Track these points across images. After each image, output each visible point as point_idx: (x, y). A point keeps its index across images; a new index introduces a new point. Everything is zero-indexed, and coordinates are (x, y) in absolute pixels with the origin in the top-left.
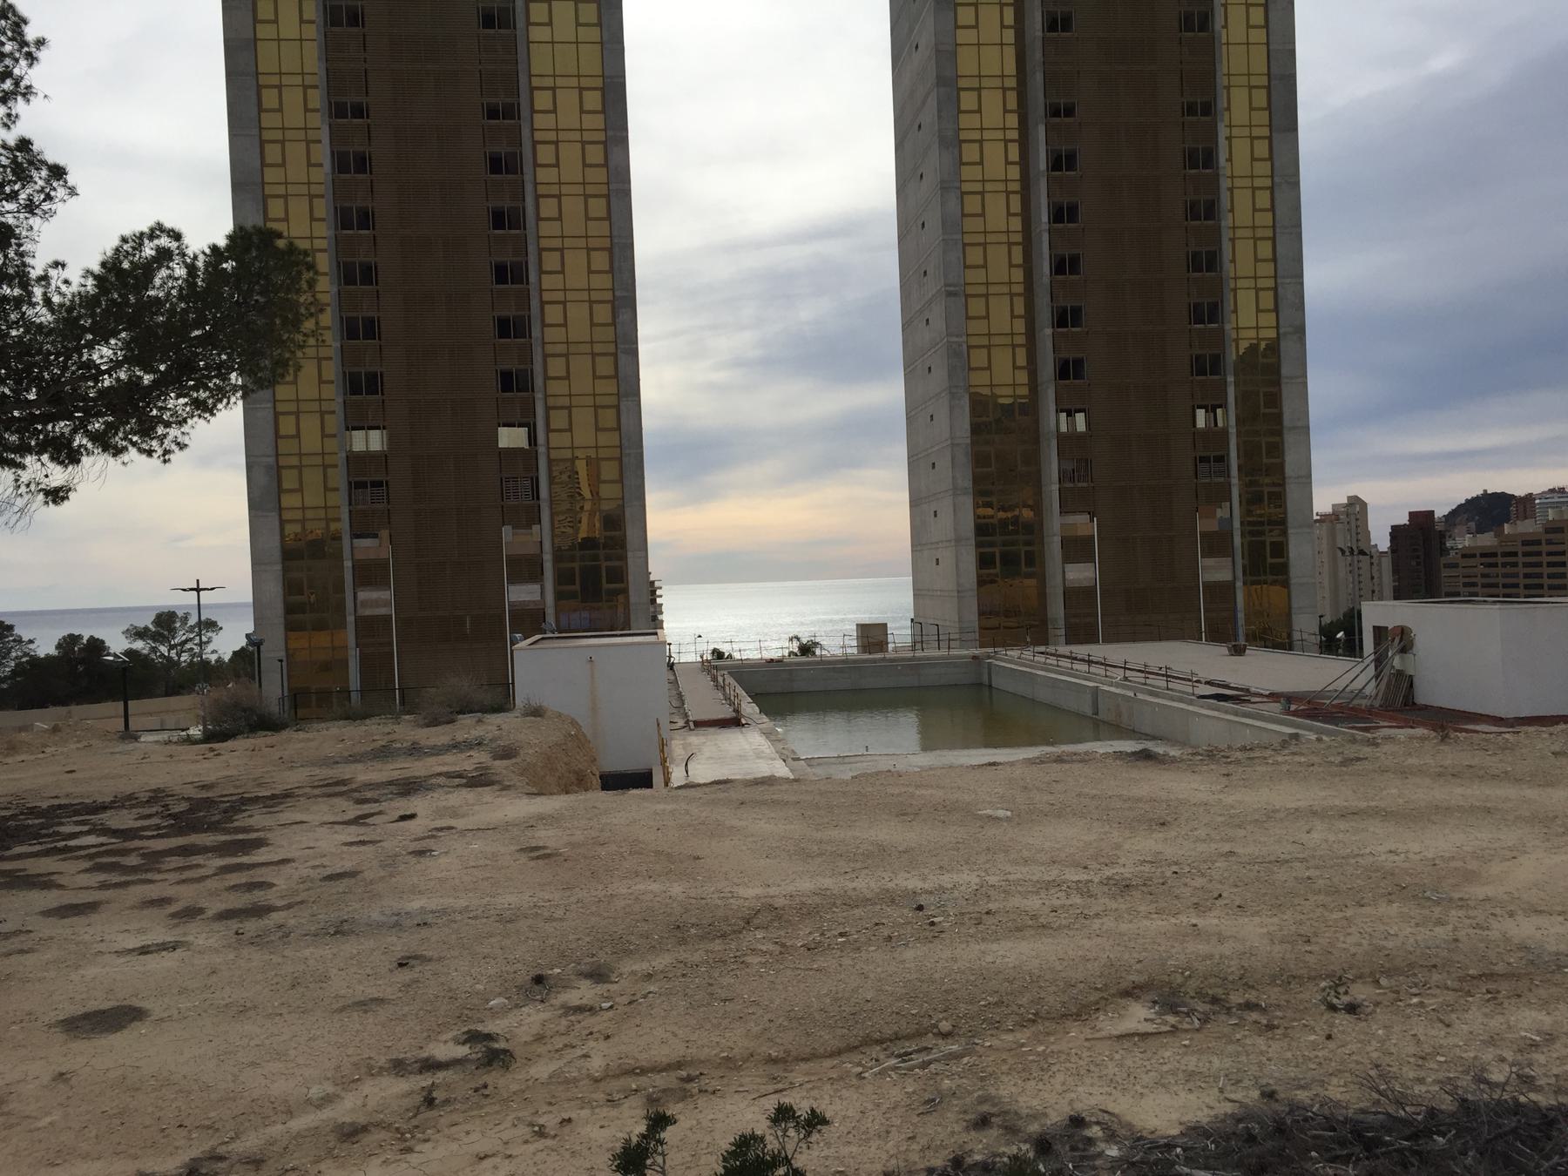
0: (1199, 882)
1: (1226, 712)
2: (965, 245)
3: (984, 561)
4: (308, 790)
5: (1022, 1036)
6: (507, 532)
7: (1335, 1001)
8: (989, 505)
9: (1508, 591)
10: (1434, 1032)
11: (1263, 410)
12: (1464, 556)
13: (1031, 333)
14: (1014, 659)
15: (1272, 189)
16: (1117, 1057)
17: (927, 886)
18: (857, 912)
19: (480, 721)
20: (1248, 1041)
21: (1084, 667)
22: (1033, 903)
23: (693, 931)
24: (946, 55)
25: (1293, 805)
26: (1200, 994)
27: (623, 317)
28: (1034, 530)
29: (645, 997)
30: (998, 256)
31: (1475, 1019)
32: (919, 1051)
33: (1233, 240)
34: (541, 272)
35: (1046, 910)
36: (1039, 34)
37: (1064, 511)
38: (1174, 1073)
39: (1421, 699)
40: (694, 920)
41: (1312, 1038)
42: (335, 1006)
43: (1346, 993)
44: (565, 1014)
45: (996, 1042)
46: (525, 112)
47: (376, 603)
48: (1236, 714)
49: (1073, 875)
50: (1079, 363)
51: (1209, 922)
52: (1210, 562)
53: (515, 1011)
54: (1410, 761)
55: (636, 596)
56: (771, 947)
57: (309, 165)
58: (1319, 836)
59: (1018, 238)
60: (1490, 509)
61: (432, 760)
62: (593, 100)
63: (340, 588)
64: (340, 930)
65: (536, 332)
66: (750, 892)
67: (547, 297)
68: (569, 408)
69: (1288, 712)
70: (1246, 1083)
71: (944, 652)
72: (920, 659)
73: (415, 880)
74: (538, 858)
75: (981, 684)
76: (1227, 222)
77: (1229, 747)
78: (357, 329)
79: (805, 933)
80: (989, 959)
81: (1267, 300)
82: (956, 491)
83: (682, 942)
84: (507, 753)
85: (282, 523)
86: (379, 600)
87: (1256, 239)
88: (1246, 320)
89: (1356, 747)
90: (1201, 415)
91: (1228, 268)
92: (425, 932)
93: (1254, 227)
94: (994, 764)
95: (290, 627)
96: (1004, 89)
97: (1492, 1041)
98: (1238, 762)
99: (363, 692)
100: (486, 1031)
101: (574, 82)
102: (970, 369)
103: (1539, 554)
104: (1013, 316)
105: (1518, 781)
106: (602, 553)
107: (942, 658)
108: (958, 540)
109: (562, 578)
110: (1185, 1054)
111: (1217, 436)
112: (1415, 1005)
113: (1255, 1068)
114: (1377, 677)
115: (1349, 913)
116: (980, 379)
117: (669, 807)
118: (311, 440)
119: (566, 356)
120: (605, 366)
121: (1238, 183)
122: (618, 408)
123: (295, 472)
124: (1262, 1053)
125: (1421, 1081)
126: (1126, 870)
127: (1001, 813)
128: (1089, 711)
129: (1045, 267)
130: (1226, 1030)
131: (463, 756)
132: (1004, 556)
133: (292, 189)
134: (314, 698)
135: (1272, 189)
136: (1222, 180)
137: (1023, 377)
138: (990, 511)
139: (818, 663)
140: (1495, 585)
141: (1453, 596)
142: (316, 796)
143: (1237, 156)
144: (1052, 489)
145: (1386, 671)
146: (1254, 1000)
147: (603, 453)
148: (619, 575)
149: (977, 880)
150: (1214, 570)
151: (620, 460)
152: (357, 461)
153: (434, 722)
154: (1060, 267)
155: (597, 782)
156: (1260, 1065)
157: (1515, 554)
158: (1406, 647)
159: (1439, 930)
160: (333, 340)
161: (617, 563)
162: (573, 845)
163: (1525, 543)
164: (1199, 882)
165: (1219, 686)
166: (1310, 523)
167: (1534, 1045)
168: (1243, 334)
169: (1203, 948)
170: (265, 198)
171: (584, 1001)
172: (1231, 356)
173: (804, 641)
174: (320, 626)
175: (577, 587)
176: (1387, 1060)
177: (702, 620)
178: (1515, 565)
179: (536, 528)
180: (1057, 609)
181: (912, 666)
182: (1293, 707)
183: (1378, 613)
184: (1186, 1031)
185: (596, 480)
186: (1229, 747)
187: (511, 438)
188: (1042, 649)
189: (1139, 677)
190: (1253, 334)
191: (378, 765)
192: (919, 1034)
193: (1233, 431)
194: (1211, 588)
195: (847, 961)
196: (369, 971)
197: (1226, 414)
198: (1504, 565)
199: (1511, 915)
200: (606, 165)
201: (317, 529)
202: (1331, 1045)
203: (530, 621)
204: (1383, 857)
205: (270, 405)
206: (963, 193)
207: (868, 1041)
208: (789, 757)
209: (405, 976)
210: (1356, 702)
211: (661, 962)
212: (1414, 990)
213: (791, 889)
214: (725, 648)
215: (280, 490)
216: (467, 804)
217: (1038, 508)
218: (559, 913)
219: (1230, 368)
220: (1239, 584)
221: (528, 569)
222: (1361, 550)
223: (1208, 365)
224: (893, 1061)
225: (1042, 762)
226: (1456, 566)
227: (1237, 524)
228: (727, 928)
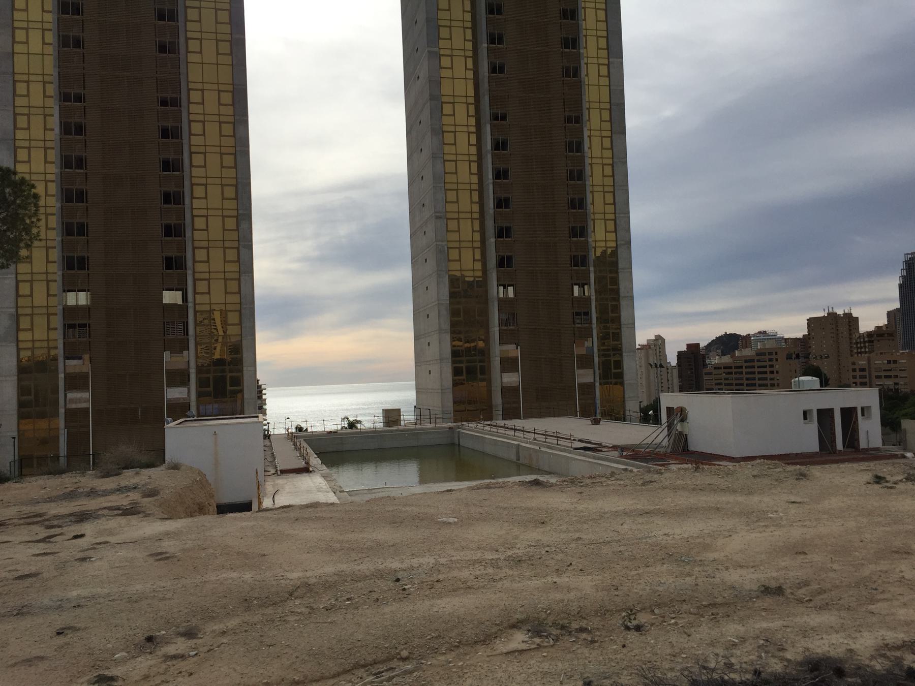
1: (589, 457)
2: (446, 190)
3: (456, 372)
4: (15, 521)
5: (450, 657)
6: (167, 355)
7: (629, 624)
9: (738, 387)
10: (682, 640)
12: (715, 368)
13: (483, 241)
14: (474, 429)
15: (612, 165)
16: (504, 666)
17: (404, 566)
18: (360, 584)
19: (137, 473)
20: (579, 651)
21: (512, 433)
22: (465, 574)
23: (255, 602)
24: (435, 82)
25: (614, 510)
26: (554, 624)
27: (243, 225)
28: (484, 354)
29: (219, 646)
30: (465, 197)
31: (704, 631)
32: (387, 670)
33: (592, 192)
35: (472, 577)
36: (486, 74)
37: (502, 343)
38: (535, 673)
39: (692, 448)
40: (256, 595)
41: (615, 647)
42: (10, 663)
43: (635, 619)
44: (165, 661)
45: (434, 661)
46: (184, 102)
47: (80, 400)
48: (594, 458)
49: (489, 556)
50: (509, 258)
51: (563, 580)
52: (581, 371)
53: (132, 661)
54: (679, 482)
56: (303, 610)
57: (45, 129)
58: (627, 527)
59: (476, 187)
60: (728, 342)
61: (102, 499)
62: (227, 98)
63: (56, 391)
64: (21, 612)
65: (188, 234)
66: (295, 575)
69: (622, 456)
70: (576, 677)
71: (432, 426)
73: (76, 577)
74: (160, 559)
75: (453, 444)
76: (589, 182)
77: (583, 477)
78: (72, 230)
79: (326, 599)
80: (435, 609)
81: (611, 226)
82: (440, 331)
83: (248, 609)
84: (152, 493)
85: (19, 350)
86: (82, 399)
88: (600, 236)
89: (650, 475)
90: (576, 288)
91: (590, 208)
92: (78, 611)
94: (450, 490)
95: (22, 416)
96: (468, 104)
97: (712, 644)
99: (68, 456)
100: (110, 675)
101: (215, 87)
102: (449, 260)
103: (754, 367)
104: (473, 231)
105: (735, 492)
106: (227, 368)
107: (433, 428)
108: (441, 360)
109: (201, 383)
110: (543, 661)
111: (584, 301)
112: (673, 624)
113: (581, 667)
115: (641, 571)
116: (455, 266)
117: (251, 524)
118: (40, 298)
119: (208, 248)
120: (231, 255)
122: (239, 280)
123: (28, 318)
124: (586, 658)
125: (672, 669)
127: (451, 520)
128: (514, 458)
129: (490, 204)
130: (569, 645)
132: (467, 368)
133: (33, 144)
134: (35, 461)
135: (612, 165)
137: (479, 266)
139: (356, 433)
140: (731, 384)
141: (710, 390)
142: (20, 525)
143: (594, 148)
144: (495, 330)
146: (584, 626)
147: (229, 307)
148: (238, 381)
149: (433, 561)
150: (584, 376)
151: (240, 311)
152: (70, 312)
153: (107, 475)
156: (585, 665)
157: (741, 367)
158: (683, 420)
159: (688, 579)
160: (55, 236)
162: (184, 550)
163: (746, 361)
165: (586, 442)
166: (633, 350)
167: (735, 645)
169: (558, 596)
170: (15, 149)
171: (179, 652)
172: (592, 256)
173: (351, 419)
174: (42, 415)
175: (211, 389)
176: (655, 658)
177: (288, 408)
178: (742, 373)
179: (185, 353)
180: (497, 399)
181: (413, 433)
182: (625, 454)
183: (670, 400)
184: (546, 647)
185: (225, 323)
186: (583, 477)
187: (170, 297)
188: (489, 422)
190: (603, 244)
191: (65, 503)
192: (389, 659)
193: (593, 298)
195: (349, 616)
196: (37, 639)
197: (590, 289)
198: (736, 373)
199: (727, 569)
200: (234, 136)
201: (41, 354)
202: (625, 651)
203: (180, 410)
205: (14, 276)
206: (445, 161)
207: (357, 666)
209: (61, 640)
211: (232, 623)
212: (673, 615)
213: (320, 572)
214: (303, 425)
215: (18, 329)
216: (120, 527)
217: (487, 340)
218: (169, 595)
219: (591, 262)
220: (597, 384)
221: (179, 378)
222: (661, 364)
223: (580, 261)
224: (371, 678)
226: (710, 374)
227: (596, 350)
228: (272, 601)
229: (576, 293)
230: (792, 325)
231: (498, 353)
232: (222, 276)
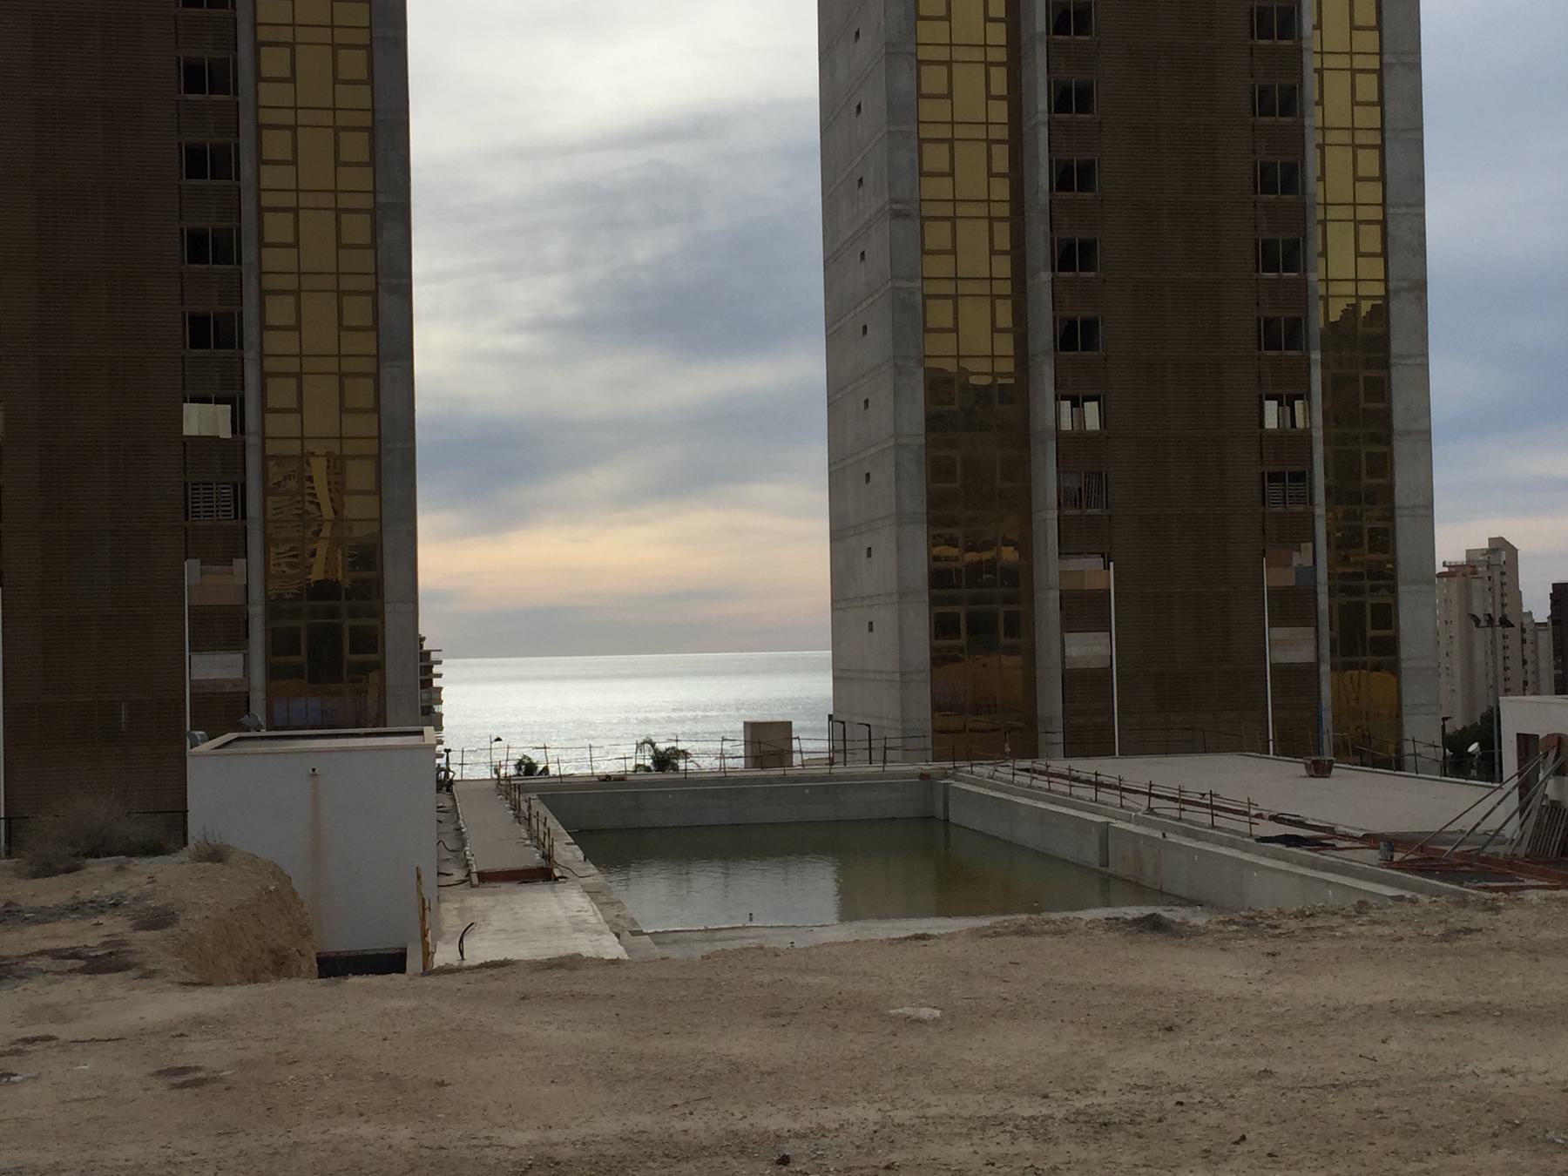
0: (1215, 1117)
1: (1300, 864)
2: (921, 141)
3: (942, 627)
6: (192, 569)
8: (952, 542)
11: (1363, 405)
13: (1019, 279)
14: (985, 781)
19: (120, 868)
21: (1089, 792)
25: (1366, 1001)
28: (1019, 580)
30: (971, 159)
34: (260, 161)
37: (1067, 549)
48: (1313, 865)
49: (1026, 1109)
50: (1090, 326)
54: (1545, 934)
55: (397, 673)
65: (249, 253)
66: (521, 1137)
67: (268, 200)
68: (299, 376)
69: (1389, 863)
71: (876, 768)
72: (839, 778)
76: (1313, 119)
81: (1371, 239)
84: (159, 919)
87: (1356, 147)
88: (1340, 268)
89: (1467, 912)
90: (1271, 407)
91: (1314, 188)
93: (1353, 129)
94: (923, 937)
98: (1290, 935)
104: (993, 252)
109: (280, 643)
111: (1295, 441)
114: (1522, 810)
115: (1433, 1164)
116: (942, 345)
120: (357, 312)
121: (1330, 61)
122: (376, 377)
126: (1105, 1100)
127: (925, 1013)
131: (86, 924)
135: (1380, 73)
136: (1306, 57)
137: (1005, 345)
138: (953, 552)
145: (1536, 802)
148: (370, 641)
150: (1289, 646)
154: (1064, 178)
155: (309, 963)
161: (942, 592)
164: (1215, 1117)
166: (1427, 575)
168: (1335, 289)
172: (1317, 322)
175: (302, 658)
177: (499, 713)
179: (239, 563)
180: (1051, 703)
181: (823, 787)
182: (1397, 857)
185: (338, 487)
186: (1280, 912)
187: (203, 420)
188: (1027, 764)
189: (1170, 809)
190: (1349, 288)
193: (1318, 434)
194: (1285, 673)
197: (1308, 410)
203: (224, 712)
204: (1491, 1079)
206: (920, 63)
208: (624, 930)
210: (1490, 849)
214: (537, 757)
217: (1025, 547)
219: (1315, 340)
220: (1325, 668)
221: (223, 629)
222: (1503, 617)
223: (1284, 333)
225: (997, 934)
229: (1271, 422)
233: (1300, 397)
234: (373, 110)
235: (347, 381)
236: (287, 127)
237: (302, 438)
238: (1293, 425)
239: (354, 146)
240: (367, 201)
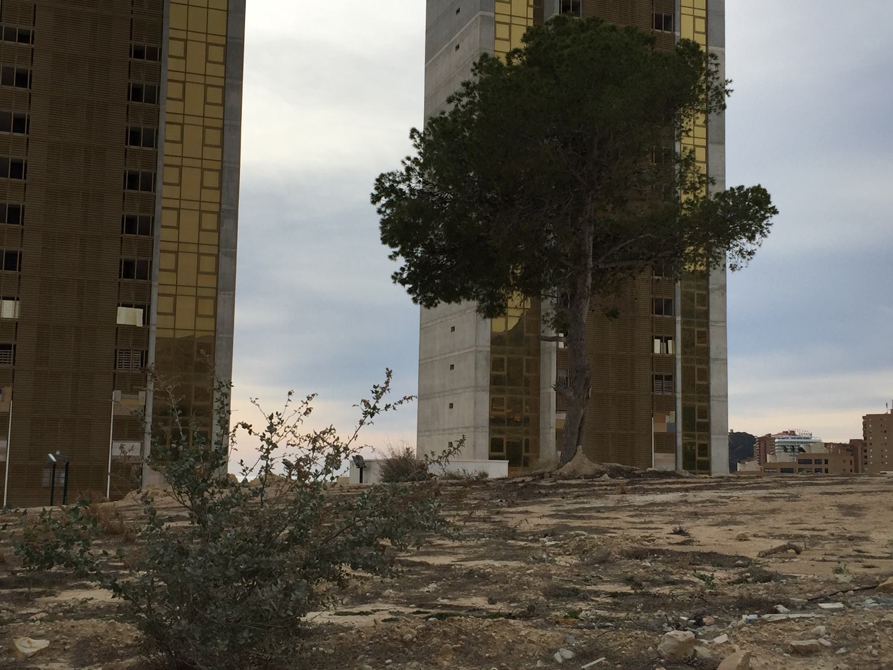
52: (660, 456)
62: (217, 54)
90: (657, 342)
122: (216, 299)
161: (496, 427)
187: (128, 316)
193: (679, 357)
221: (130, 428)
229: (657, 349)
230: (840, 426)
231: (553, 422)
232: (192, 291)
233: (671, 338)
234: (222, 161)
235: (200, 301)
236: (177, 166)
237: (174, 329)
238: (667, 352)
239: (212, 179)
240: (215, 208)
